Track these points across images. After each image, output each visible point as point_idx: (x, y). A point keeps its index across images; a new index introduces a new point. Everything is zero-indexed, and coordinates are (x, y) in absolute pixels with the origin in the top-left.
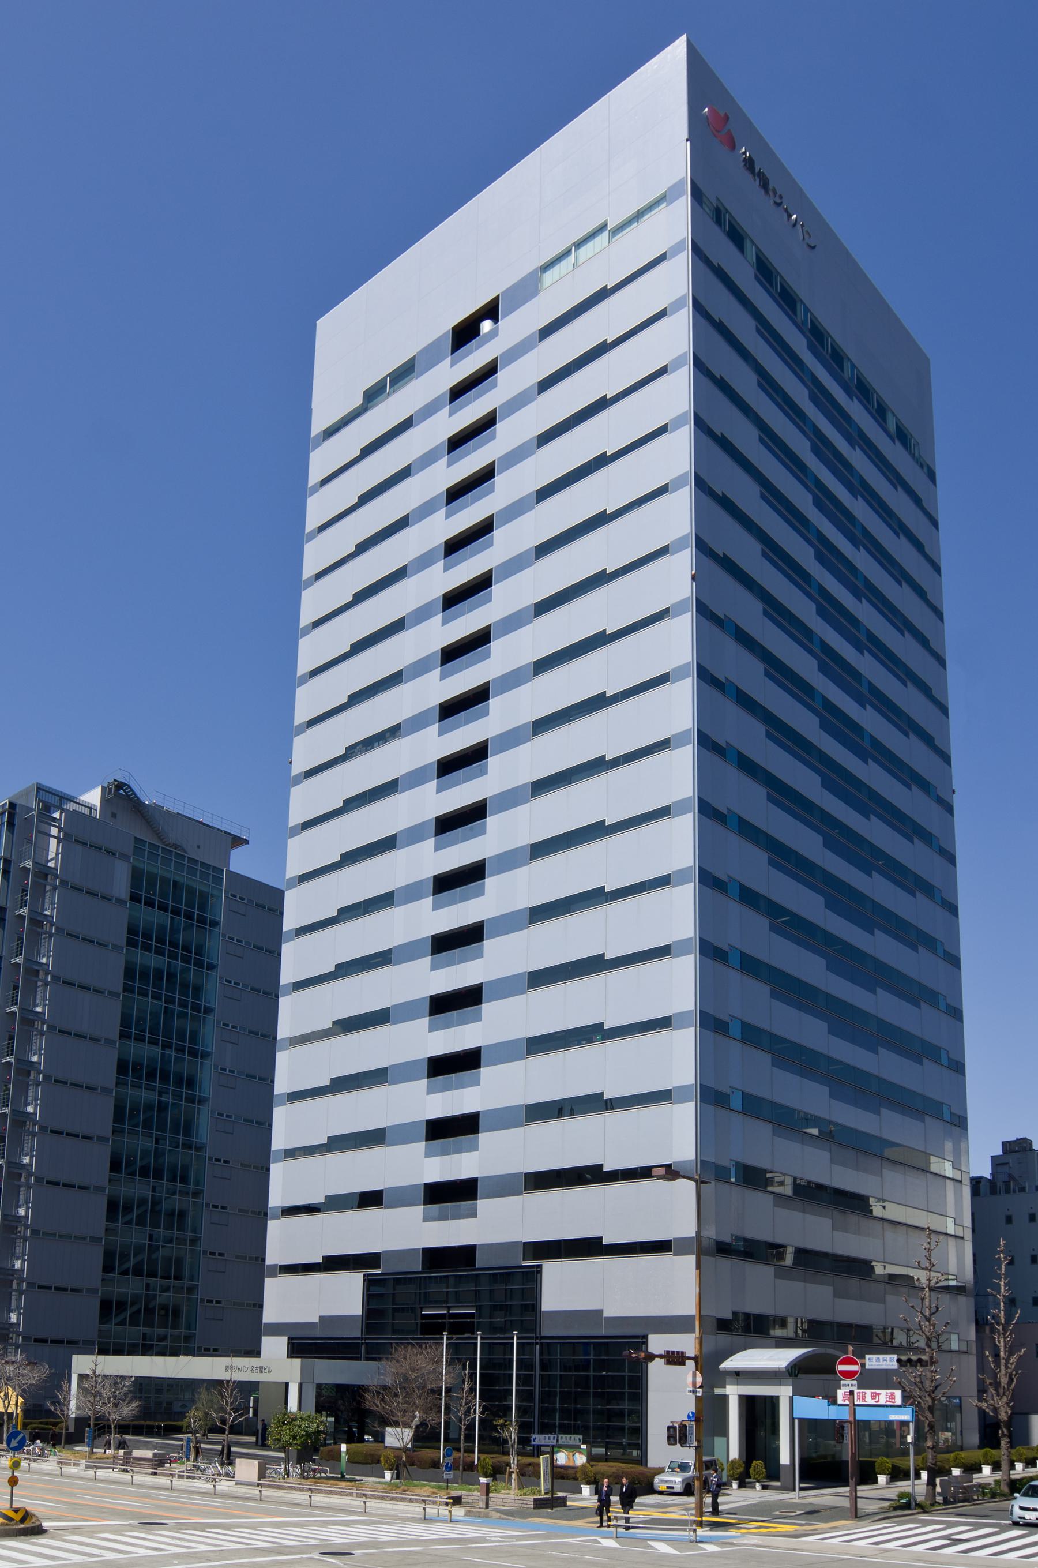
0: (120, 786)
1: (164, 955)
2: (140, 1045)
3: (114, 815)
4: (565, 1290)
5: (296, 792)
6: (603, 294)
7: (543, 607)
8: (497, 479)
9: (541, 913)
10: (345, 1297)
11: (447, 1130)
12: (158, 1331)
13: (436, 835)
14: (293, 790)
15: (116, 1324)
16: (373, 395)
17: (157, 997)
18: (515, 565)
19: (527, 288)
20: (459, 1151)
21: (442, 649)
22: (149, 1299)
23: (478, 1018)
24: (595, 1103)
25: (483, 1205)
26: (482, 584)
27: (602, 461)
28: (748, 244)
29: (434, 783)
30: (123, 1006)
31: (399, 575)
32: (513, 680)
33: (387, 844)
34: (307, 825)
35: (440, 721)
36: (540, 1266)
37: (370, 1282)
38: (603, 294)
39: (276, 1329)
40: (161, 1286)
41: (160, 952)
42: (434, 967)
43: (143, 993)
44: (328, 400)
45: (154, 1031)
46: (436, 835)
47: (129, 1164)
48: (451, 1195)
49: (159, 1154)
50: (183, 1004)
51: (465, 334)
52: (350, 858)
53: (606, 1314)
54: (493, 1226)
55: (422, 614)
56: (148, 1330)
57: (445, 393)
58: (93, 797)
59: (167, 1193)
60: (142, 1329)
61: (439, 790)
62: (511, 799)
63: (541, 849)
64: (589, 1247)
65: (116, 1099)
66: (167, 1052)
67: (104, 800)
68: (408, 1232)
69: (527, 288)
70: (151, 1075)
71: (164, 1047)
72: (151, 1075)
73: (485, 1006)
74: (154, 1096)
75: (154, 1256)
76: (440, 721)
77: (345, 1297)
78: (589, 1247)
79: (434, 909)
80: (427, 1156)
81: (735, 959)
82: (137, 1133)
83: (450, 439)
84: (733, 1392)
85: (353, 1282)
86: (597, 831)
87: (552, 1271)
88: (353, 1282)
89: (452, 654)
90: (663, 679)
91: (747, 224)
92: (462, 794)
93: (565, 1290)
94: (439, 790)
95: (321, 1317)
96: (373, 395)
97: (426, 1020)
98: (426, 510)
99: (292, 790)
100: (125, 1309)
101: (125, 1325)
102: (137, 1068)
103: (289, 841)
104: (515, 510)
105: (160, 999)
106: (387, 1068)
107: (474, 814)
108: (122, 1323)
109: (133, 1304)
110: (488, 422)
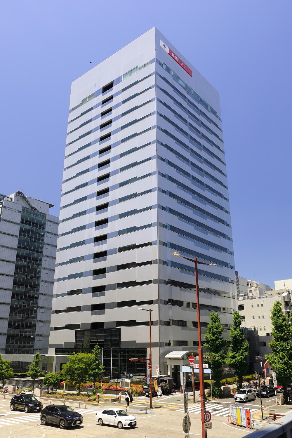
0: (19, 193)
1: (31, 226)
2: (23, 250)
3: (18, 200)
4: (127, 335)
5: (69, 126)
6: (137, 82)
7: (123, 114)
8: (113, 111)
9: (123, 141)
10: (70, 336)
11: (98, 290)
12: (25, 330)
13: (95, 226)
14: (66, 148)
15: (13, 328)
16: (84, 101)
17: (28, 237)
18: (116, 131)
19: (119, 80)
20: (102, 244)
21: (99, 164)
22: (23, 321)
23: (106, 243)
24: (133, 284)
25: (106, 311)
26: (108, 148)
27: (136, 108)
28: (171, 71)
29: (97, 169)
30: (17, 252)
31: (91, 120)
32: (115, 158)
33: (85, 198)
34: (65, 207)
35: (97, 196)
36: (120, 328)
37: (77, 332)
38: (137, 82)
39: (52, 346)
40: (26, 317)
41: (30, 225)
42: (92, 314)
43: (25, 236)
44: (74, 102)
45: (27, 246)
46: (95, 226)
47: (14, 325)
48: (98, 308)
49: (27, 279)
50: (35, 238)
51: (106, 89)
52: (76, 202)
53: (137, 342)
54: (110, 316)
55: (94, 155)
56: (22, 330)
57: (95, 207)
58: (13, 196)
59: (29, 290)
60: (19, 344)
61: (96, 215)
62: (115, 187)
63: (122, 155)
64: (132, 323)
65: (12, 291)
66: (31, 251)
67: (16, 196)
68: (87, 318)
69: (119, 80)
70: (26, 258)
71: (30, 250)
72: (26, 258)
73: (107, 256)
74: (25, 277)
75: (23, 322)
76: (97, 196)
77: (70, 336)
78: (132, 323)
79: (97, 185)
80: (91, 315)
81: (169, 245)
82: (21, 274)
83: (102, 101)
84: (168, 363)
85: (73, 332)
86: (134, 212)
87: (124, 329)
88: (73, 332)
89: (101, 165)
90: (150, 159)
91: (171, 67)
92: (102, 201)
93: (127, 335)
94: (96, 215)
95: (64, 342)
96: (84, 101)
97: (93, 260)
98: (95, 130)
99: (67, 136)
100: (14, 339)
101: (14, 343)
102: (22, 256)
103: (64, 172)
104: (117, 106)
105: (29, 237)
106: (81, 290)
107: (105, 206)
108: (13, 343)
109: (16, 337)
110: (111, 98)
